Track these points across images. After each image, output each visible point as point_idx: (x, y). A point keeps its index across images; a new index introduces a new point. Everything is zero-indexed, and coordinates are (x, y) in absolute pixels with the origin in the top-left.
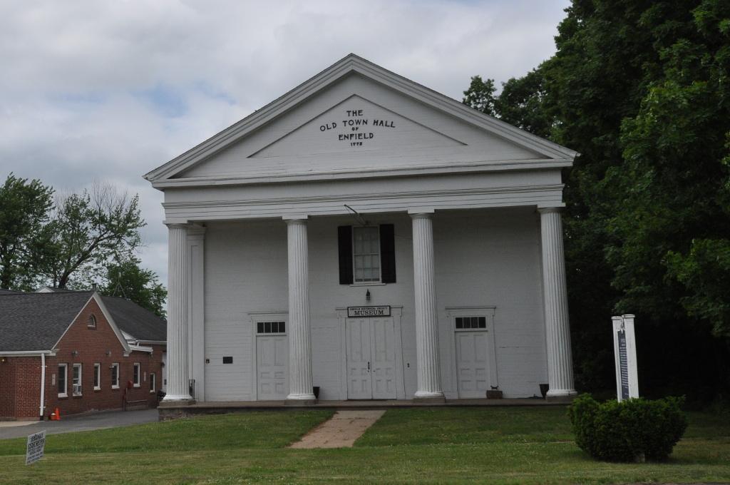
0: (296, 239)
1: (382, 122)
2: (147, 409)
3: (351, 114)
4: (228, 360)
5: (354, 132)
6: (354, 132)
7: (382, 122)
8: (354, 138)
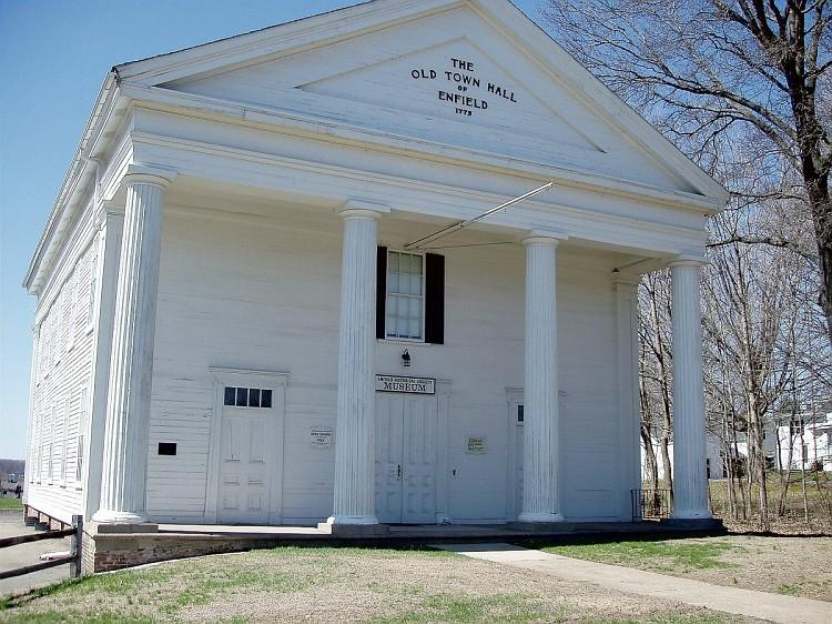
0: (541, 271)
1: (499, 89)
2: (481, 603)
3: (458, 64)
4: (167, 449)
5: (461, 93)
6: (461, 93)
7: (499, 89)
8: (460, 101)
